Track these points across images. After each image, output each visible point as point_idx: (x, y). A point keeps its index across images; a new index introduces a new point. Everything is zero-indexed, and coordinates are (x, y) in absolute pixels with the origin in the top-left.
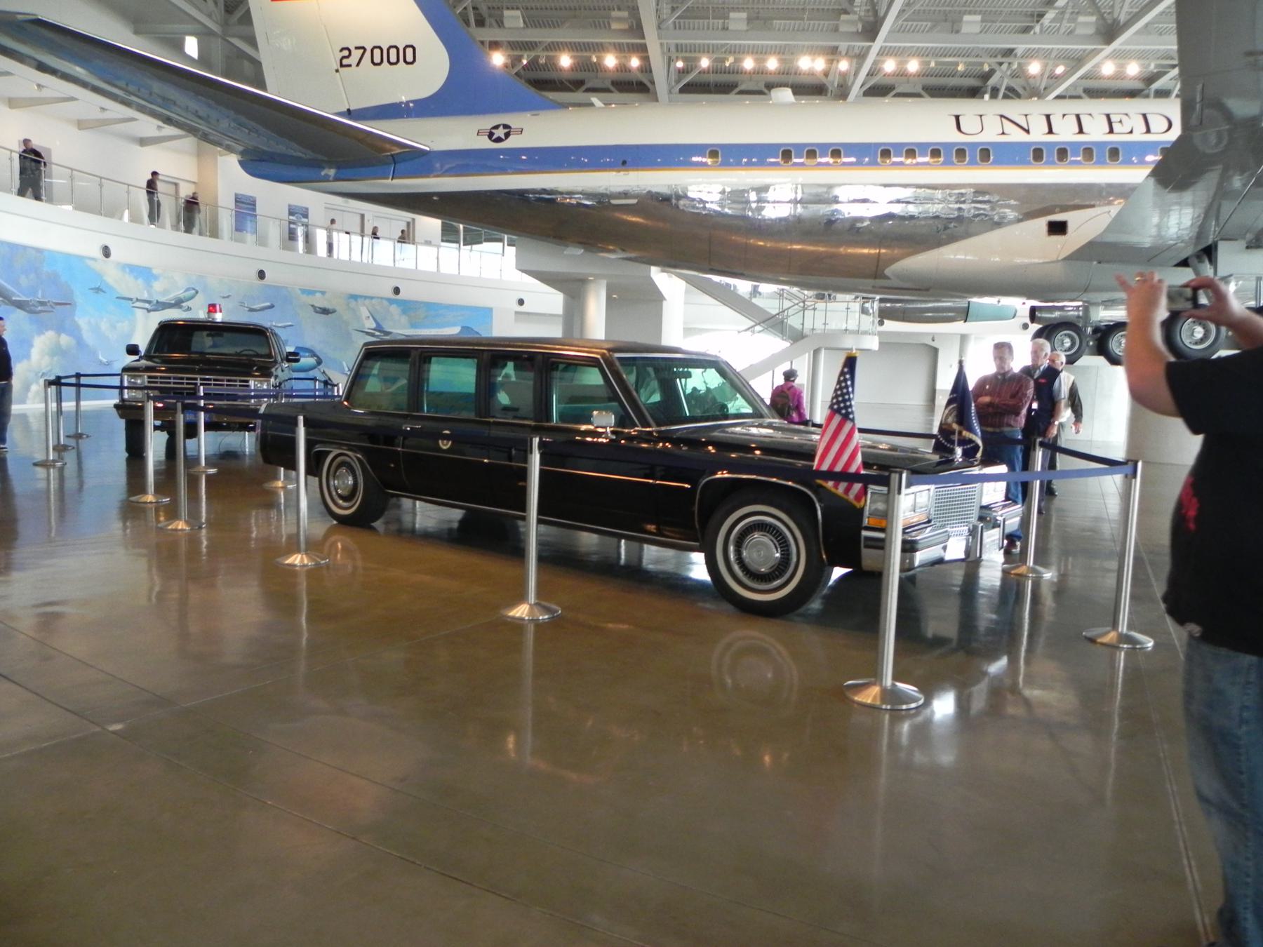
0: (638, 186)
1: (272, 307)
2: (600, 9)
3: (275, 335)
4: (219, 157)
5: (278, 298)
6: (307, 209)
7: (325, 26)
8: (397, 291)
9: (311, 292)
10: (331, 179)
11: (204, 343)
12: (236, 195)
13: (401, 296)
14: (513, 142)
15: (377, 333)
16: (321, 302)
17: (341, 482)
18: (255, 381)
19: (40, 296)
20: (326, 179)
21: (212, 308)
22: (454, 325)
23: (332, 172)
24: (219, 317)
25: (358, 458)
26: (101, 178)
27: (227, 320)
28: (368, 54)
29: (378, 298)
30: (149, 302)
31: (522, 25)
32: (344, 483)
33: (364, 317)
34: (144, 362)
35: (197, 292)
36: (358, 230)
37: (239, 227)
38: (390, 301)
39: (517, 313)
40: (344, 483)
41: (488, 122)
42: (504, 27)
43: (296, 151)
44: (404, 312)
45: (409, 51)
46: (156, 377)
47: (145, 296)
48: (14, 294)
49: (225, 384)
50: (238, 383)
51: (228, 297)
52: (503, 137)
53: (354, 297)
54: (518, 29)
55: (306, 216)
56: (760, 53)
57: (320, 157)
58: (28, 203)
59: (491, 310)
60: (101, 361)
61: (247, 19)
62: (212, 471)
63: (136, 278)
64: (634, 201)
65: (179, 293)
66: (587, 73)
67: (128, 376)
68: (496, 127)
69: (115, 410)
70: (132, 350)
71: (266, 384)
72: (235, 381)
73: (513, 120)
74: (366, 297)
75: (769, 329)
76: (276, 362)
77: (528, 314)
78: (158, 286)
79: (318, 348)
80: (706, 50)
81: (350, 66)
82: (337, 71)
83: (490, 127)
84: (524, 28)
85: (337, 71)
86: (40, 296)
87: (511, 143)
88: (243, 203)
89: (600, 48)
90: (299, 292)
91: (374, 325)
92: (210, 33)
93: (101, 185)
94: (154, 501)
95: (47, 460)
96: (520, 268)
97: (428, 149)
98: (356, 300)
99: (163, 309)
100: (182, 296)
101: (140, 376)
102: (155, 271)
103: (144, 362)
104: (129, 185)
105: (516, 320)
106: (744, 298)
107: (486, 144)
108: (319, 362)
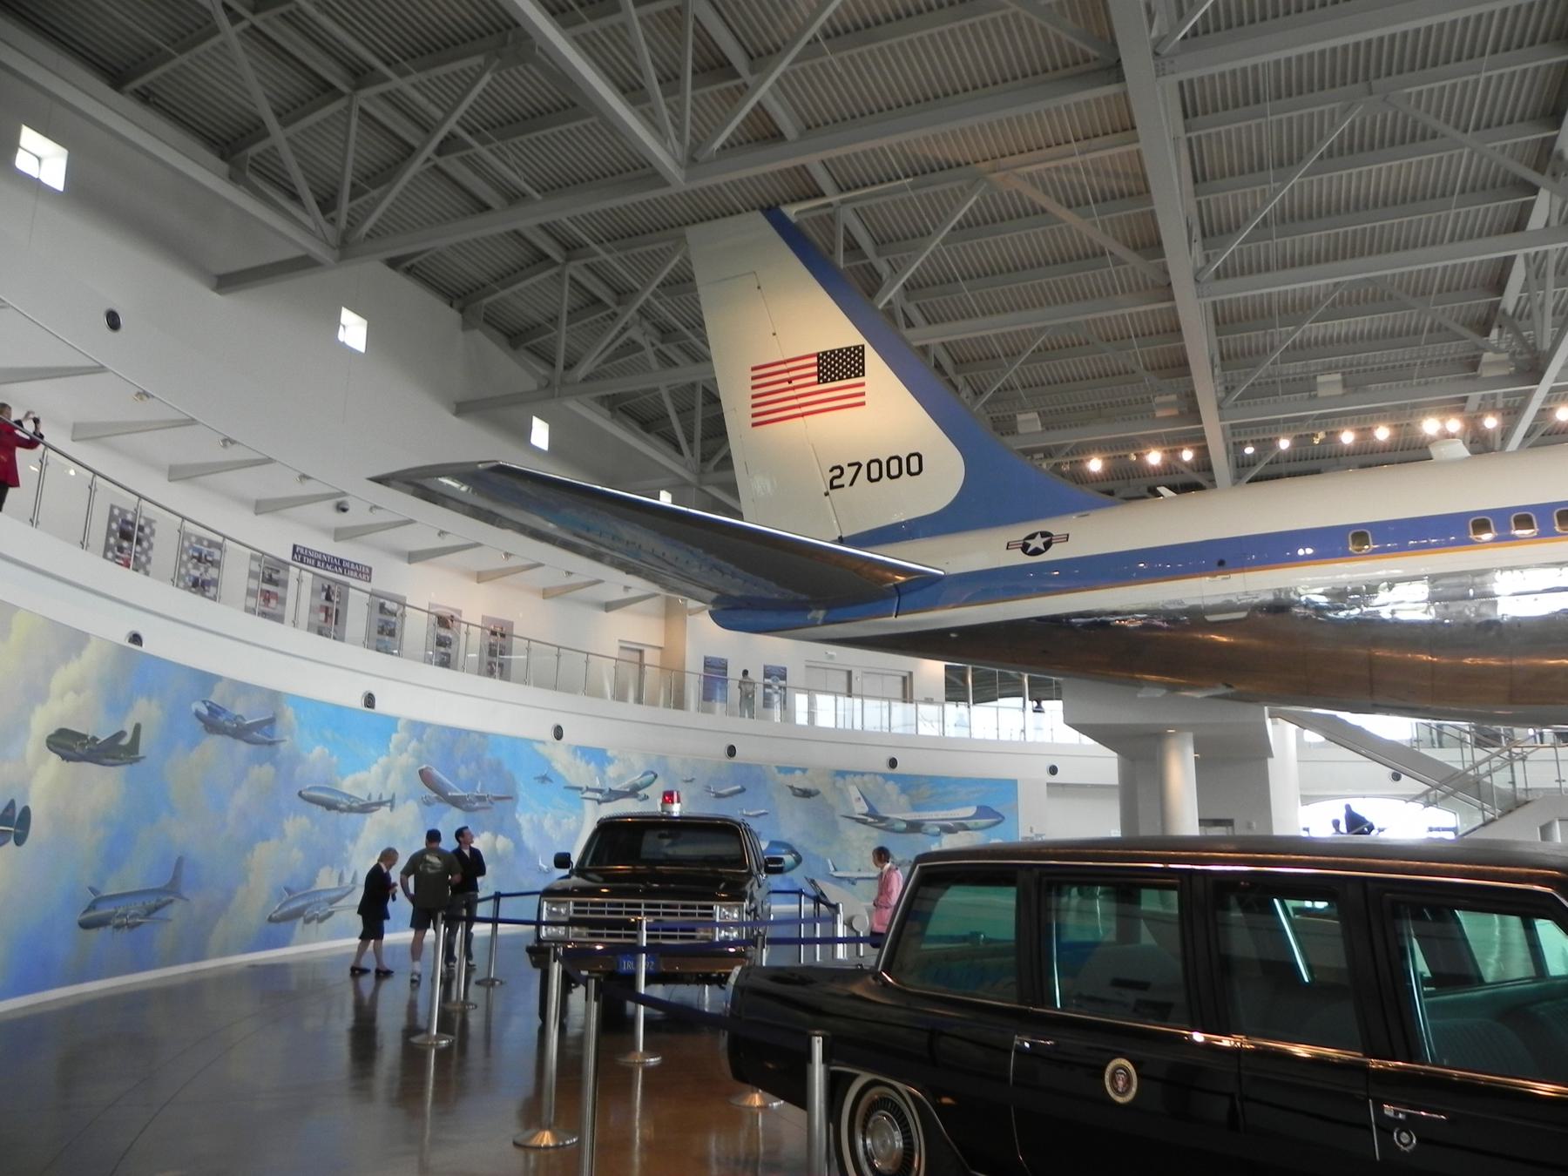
0: (1246, 593)
1: (742, 790)
2: (1131, 404)
3: (749, 831)
4: (688, 617)
5: (749, 780)
6: (785, 669)
7: (813, 445)
8: (893, 763)
9: (789, 770)
10: (819, 622)
11: (653, 845)
12: (706, 658)
13: (898, 770)
14: (1056, 553)
15: (870, 820)
16: (801, 782)
17: (878, 1143)
18: (721, 906)
19: (478, 789)
20: (813, 624)
21: (668, 797)
22: (968, 805)
23: (821, 614)
24: (676, 809)
25: (911, 1094)
26: (559, 647)
27: (685, 813)
28: (864, 470)
29: (870, 773)
30: (600, 791)
31: (1040, 429)
32: (884, 1145)
33: (853, 798)
34: (576, 880)
35: (656, 776)
36: (845, 690)
37: (708, 696)
38: (886, 777)
39: (1048, 785)
40: (884, 1145)
41: (1019, 532)
42: (1018, 433)
43: (773, 592)
44: (904, 791)
45: (914, 460)
46: (585, 904)
47: (597, 784)
48: (451, 789)
49: (677, 911)
50: (697, 911)
51: (691, 781)
52: (1043, 548)
53: (842, 774)
54: (1037, 433)
55: (784, 678)
56: (1363, 420)
57: (804, 597)
58: (493, 685)
59: (1014, 783)
60: (541, 869)
61: (727, 462)
62: (653, 1061)
63: (588, 763)
64: (1242, 615)
65: (636, 778)
66: (1111, 482)
67: (548, 902)
68: (1032, 537)
69: (527, 954)
70: (562, 861)
71: (736, 910)
72: (694, 907)
73: (1055, 526)
74: (856, 774)
75: (1460, 794)
76: (750, 874)
77: (1063, 785)
78: (612, 771)
79: (797, 843)
80: (1286, 426)
81: (842, 486)
82: (827, 494)
83: (1023, 538)
84: (1043, 431)
85: (827, 494)
86: (478, 791)
87: (1055, 553)
88: (713, 667)
89: (1140, 444)
90: (776, 770)
91: (866, 809)
92: (686, 484)
93: (558, 656)
94: (551, 1144)
95: (488, 979)
96: (1070, 722)
97: (942, 573)
98: (844, 778)
99: (616, 799)
100: (638, 782)
101: (565, 902)
102: (609, 753)
103: (576, 880)
104: (588, 654)
105: (1050, 794)
106: (1404, 746)
107: (1019, 558)
108: (798, 860)
